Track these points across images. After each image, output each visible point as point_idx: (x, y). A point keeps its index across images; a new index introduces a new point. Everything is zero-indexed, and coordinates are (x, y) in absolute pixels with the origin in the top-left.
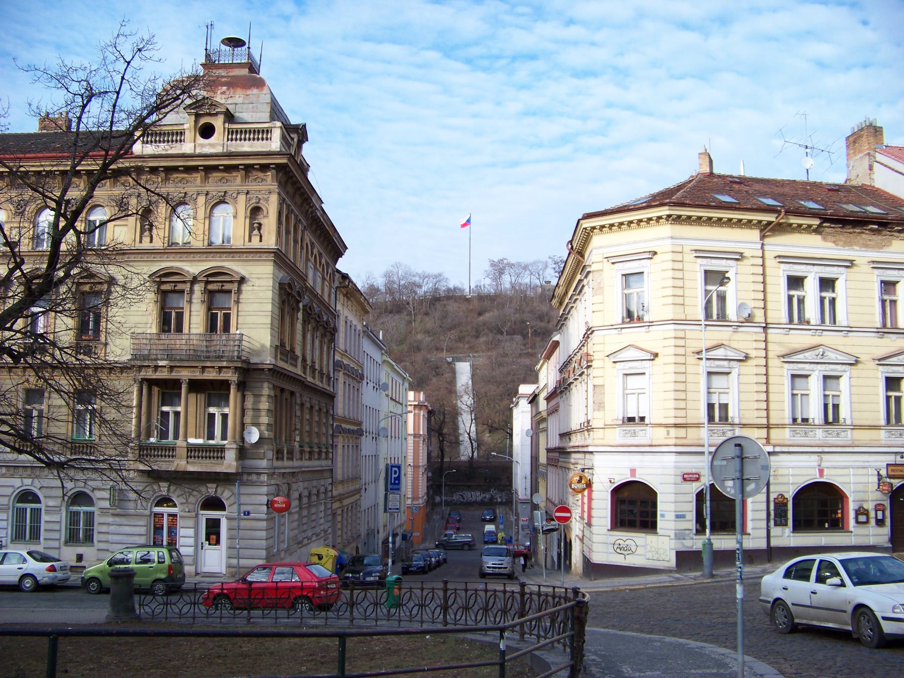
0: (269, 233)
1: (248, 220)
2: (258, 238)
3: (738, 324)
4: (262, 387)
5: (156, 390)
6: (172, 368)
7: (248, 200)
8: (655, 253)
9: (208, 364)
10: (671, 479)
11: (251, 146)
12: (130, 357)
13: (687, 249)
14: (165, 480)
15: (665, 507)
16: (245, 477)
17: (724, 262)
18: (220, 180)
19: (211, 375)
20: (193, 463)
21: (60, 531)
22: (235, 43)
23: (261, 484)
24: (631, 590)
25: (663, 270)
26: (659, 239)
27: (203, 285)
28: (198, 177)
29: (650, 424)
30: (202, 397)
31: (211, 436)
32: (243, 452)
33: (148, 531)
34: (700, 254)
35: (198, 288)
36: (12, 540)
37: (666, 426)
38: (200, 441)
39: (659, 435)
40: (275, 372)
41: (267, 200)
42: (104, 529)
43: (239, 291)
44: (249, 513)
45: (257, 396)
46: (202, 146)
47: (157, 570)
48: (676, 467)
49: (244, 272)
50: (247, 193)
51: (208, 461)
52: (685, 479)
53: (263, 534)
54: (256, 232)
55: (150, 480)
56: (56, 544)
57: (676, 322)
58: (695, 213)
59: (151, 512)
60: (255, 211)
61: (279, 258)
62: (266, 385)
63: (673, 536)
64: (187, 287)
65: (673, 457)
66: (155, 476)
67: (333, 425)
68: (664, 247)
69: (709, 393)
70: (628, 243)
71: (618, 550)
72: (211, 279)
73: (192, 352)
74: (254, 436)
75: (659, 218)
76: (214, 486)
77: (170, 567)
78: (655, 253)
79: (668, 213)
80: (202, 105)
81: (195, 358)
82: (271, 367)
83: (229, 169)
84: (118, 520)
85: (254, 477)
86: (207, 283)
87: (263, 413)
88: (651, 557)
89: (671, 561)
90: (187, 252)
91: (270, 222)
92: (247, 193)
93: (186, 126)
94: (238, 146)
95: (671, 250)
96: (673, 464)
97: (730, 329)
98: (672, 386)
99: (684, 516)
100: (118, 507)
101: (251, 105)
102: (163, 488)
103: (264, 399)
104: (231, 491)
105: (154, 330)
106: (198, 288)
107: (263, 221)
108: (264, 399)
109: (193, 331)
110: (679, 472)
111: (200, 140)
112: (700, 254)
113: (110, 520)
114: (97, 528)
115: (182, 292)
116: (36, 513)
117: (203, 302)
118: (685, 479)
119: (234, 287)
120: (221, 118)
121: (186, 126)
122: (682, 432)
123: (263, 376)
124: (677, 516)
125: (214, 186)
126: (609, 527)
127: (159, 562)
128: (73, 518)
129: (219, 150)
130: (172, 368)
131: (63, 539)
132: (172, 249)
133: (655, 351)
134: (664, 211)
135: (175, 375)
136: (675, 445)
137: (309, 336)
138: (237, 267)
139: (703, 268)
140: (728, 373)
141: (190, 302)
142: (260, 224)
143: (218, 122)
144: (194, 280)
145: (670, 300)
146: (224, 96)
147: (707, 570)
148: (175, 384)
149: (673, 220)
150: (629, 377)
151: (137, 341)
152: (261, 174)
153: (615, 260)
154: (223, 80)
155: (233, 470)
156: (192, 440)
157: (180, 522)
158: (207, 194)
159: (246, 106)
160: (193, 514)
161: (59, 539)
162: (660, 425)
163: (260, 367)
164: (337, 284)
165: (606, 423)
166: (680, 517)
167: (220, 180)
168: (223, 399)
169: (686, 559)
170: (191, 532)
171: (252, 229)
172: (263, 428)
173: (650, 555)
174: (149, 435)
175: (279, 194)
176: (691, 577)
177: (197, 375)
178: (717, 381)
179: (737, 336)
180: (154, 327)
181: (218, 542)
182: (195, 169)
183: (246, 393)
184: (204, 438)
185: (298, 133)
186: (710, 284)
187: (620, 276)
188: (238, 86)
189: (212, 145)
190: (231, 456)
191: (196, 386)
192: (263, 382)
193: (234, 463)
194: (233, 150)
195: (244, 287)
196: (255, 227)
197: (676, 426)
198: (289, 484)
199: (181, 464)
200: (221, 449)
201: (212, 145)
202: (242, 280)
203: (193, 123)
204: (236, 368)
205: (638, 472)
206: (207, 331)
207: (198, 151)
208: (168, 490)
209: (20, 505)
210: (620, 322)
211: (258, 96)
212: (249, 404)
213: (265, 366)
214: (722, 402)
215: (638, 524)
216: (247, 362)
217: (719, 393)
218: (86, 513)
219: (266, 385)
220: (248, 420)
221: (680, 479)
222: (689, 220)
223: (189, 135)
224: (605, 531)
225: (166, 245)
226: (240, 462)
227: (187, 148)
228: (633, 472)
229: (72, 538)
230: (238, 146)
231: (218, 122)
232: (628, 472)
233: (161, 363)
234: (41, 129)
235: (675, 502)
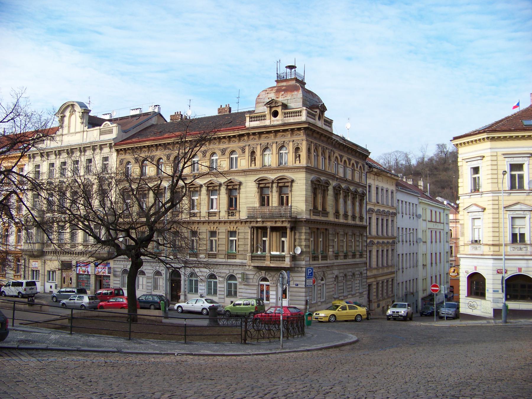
0: (303, 159)
1: (294, 154)
2: (299, 161)
3: (529, 191)
4: (302, 229)
5: (260, 231)
6: (263, 222)
7: (294, 144)
8: (484, 157)
9: (277, 220)
10: (491, 272)
11: (294, 120)
12: (247, 217)
13: (499, 154)
14: (264, 270)
15: (489, 286)
16: (296, 269)
17: (521, 159)
18: (282, 136)
19: (279, 225)
20: (273, 263)
21: (224, 291)
22: (291, 67)
23: (302, 272)
24: (458, 326)
25: (487, 166)
26: (485, 149)
27: (276, 184)
28: (272, 135)
29: (483, 244)
30: (278, 234)
31: (283, 251)
32: (294, 258)
33: (258, 292)
34: (506, 155)
35: (275, 185)
36: (207, 295)
37: (489, 245)
38: (278, 253)
39: (486, 250)
40: (308, 221)
41: (302, 144)
42: (241, 290)
43: (291, 186)
44: (298, 285)
45: (300, 233)
46: (274, 121)
47: (251, 309)
48: (493, 266)
49: (293, 178)
50: (293, 141)
51: (279, 262)
52: (498, 272)
53: (304, 294)
54: (298, 159)
55: (258, 270)
56: (223, 296)
57: (493, 192)
58: (502, 135)
59: (259, 284)
60: (297, 149)
61: (308, 170)
62: (304, 228)
63: (492, 301)
64: (270, 185)
65: (492, 261)
66: (259, 269)
67: (367, 241)
68: (487, 153)
69: (512, 228)
70: (472, 152)
71: (470, 307)
72: (279, 181)
73: (271, 215)
74: (298, 251)
75: (484, 139)
76: (264, 272)
77: (256, 307)
78: (484, 157)
79: (487, 136)
80: (272, 103)
81: (272, 217)
82: (305, 220)
83: (284, 131)
84: (246, 287)
85: (300, 269)
86: (278, 183)
87: (303, 240)
88: (483, 311)
89: (491, 314)
90: (270, 170)
91: (303, 154)
92: (293, 141)
93: (266, 113)
94: (288, 120)
95: (490, 155)
96: (492, 265)
97: (525, 194)
98: (491, 225)
99: (498, 291)
100: (246, 281)
101: (294, 100)
102: (263, 274)
103: (303, 234)
104: (271, 274)
105: (257, 205)
106: (275, 185)
107: (301, 154)
108: (303, 234)
109: (274, 205)
110: (495, 269)
111: (273, 118)
112: (506, 155)
113: (243, 287)
114: (238, 290)
115: (268, 187)
116: (215, 283)
117: (277, 191)
118: (498, 272)
119: (289, 184)
120: (280, 108)
121: (266, 113)
122: (496, 248)
123: (303, 224)
124: (494, 291)
125: (280, 139)
126: (466, 295)
127: (252, 305)
128: (230, 285)
129: (280, 122)
130: (263, 222)
131: (226, 295)
132: (265, 169)
133: (484, 207)
134: (485, 135)
135: (264, 225)
136: (492, 255)
137: (341, 201)
138: (290, 175)
139: (508, 163)
140: (525, 217)
141: (272, 192)
142: (300, 155)
143: (279, 110)
144: (273, 182)
145: (490, 181)
146: (283, 96)
147: (503, 319)
148: (264, 229)
149: (491, 139)
150: (475, 220)
151: (249, 211)
152: (298, 132)
153: (468, 160)
154: (283, 88)
155: (289, 266)
156: (274, 253)
157: (271, 288)
158: (276, 143)
159: (292, 100)
160: (275, 285)
161: (224, 295)
162: (487, 245)
163: (301, 220)
164: (366, 170)
165: (465, 243)
166: (495, 291)
167: (282, 136)
168: (284, 235)
169: (497, 312)
170: (274, 293)
171: (296, 158)
172: (303, 247)
173: (483, 310)
174: (257, 251)
175: (307, 140)
176: (500, 322)
177: (274, 225)
178: (518, 222)
179: (529, 198)
180: (258, 203)
181: (286, 298)
182: (270, 132)
183: (296, 232)
184: (280, 251)
185: (319, 109)
186: (514, 171)
187: (469, 169)
188: (289, 91)
189: (278, 120)
190: (288, 260)
191: (274, 229)
192: (302, 226)
193: (289, 263)
194: (286, 122)
195: (294, 184)
196: (298, 156)
197: (493, 245)
198: (323, 272)
199: (267, 263)
200: (284, 257)
201: (278, 120)
202: (293, 181)
203: (269, 111)
204: (289, 221)
205: (478, 268)
206: (279, 205)
207: (272, 123)
208: (265, 275)
209: (209, 280)
210: (470, 192)
211: (297, 95)
212: (297, 237)
213: (302, 220)
214: (521, 232)
215: (480, 294)
216: (296, 218)
217: (519, 228)
218: (234, 284)
219: (304, 228)
220: (297, 243)
221: (496, 272)
222: (499, 138)
223: (268, 117)
224: (465, 297)
225: (261, 167)
226: (293, 262)
227: (267, 122)
228: (476, 268)
229: (229, 294)
230: (288, 120)
231: (279, 110)
232: (474, 268)
233: (259, 220)
234: (219, 113)
235: (493, 284)
